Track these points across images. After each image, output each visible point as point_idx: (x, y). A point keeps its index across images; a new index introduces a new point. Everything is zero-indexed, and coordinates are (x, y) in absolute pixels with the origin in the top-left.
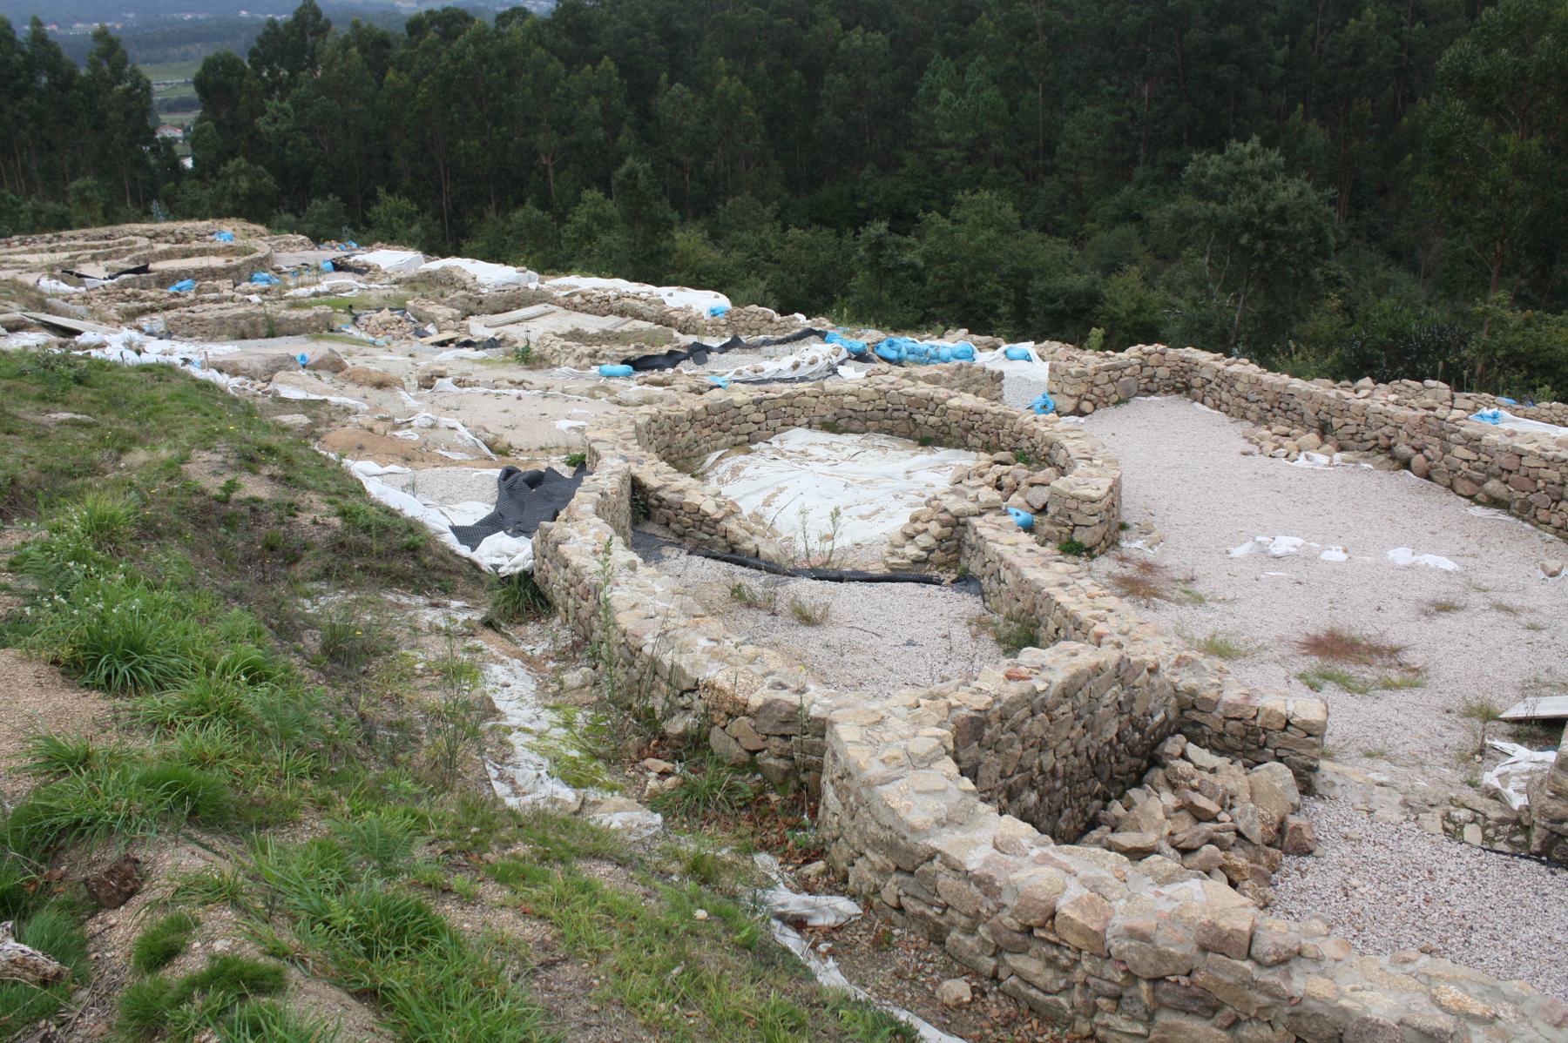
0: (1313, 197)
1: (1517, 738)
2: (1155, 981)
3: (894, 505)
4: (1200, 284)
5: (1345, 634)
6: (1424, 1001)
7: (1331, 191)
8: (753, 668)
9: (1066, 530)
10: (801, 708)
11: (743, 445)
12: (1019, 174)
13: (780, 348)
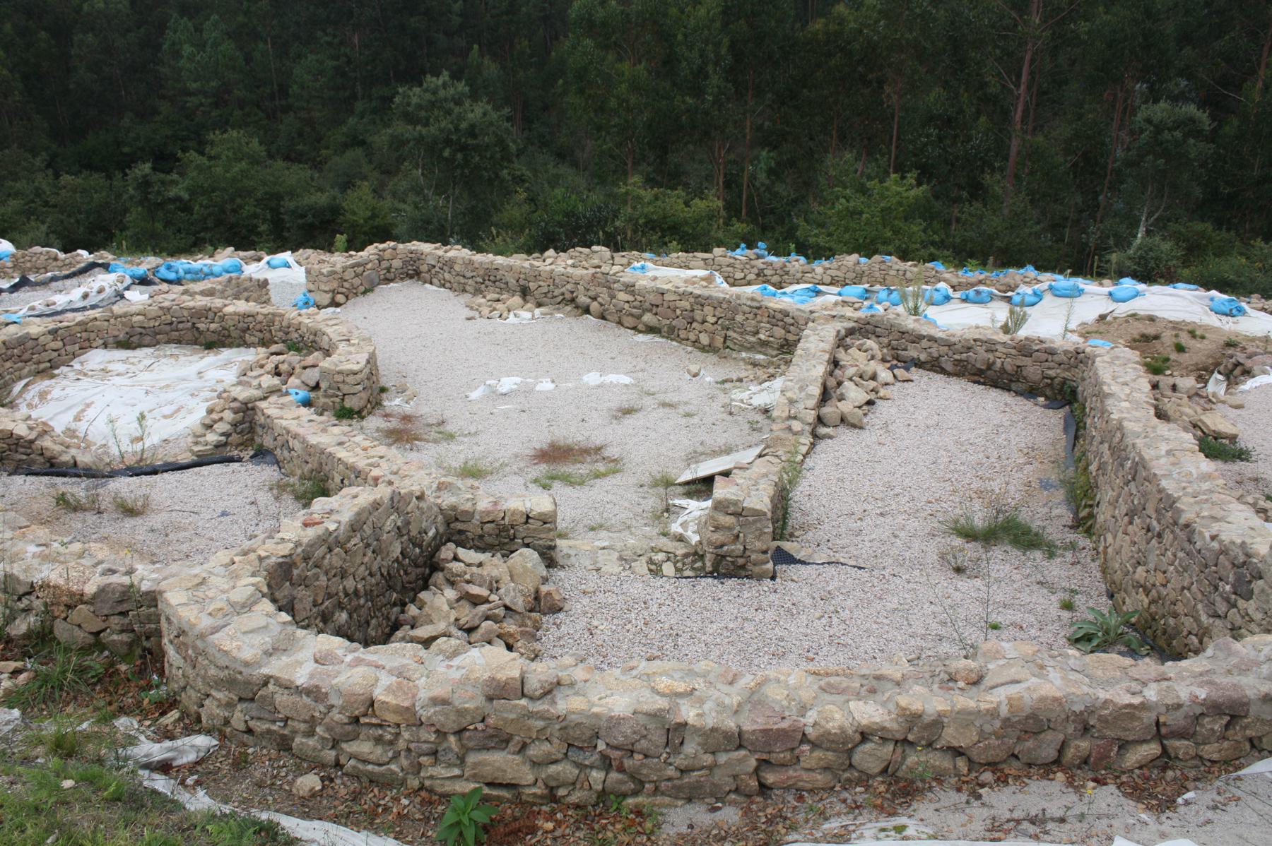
0: (494, 116)
1: (689, 495)
2: (459, 732)
3: (192, 403)
4: (418, 191)
5: (562, 443)
6: (647, 693)
7: (506, 111)
8: (83, 561)
9: (337, 400)
10: (132, 586)
11: (47, 370)
12: (261, 114)
13: (68, 282)
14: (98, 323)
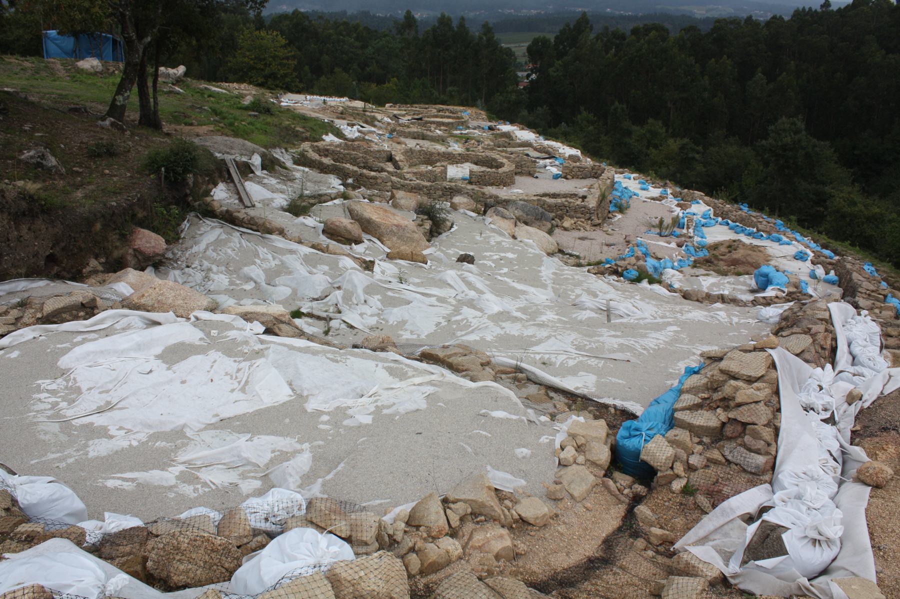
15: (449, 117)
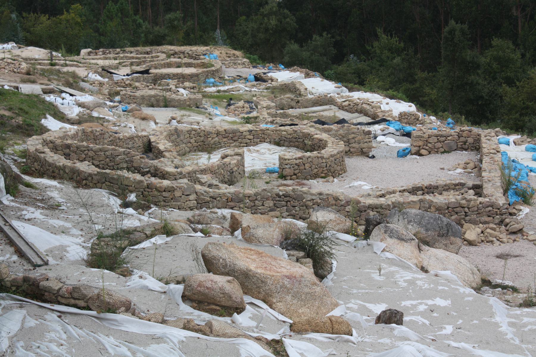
14: (269, 131)
15: (189, 65)
